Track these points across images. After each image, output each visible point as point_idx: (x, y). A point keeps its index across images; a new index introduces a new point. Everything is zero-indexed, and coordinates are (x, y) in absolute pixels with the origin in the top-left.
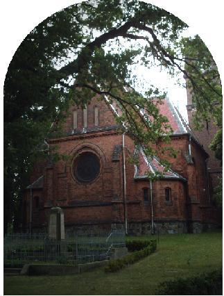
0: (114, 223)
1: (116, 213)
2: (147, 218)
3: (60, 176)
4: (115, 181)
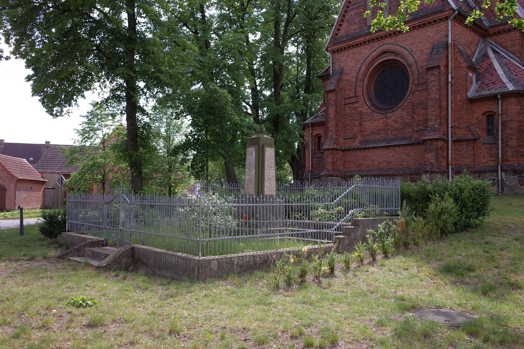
0: (426, 172)
1: (431, 157)
2: (492, 164)
3: (347, 101)
4: (431, 103)
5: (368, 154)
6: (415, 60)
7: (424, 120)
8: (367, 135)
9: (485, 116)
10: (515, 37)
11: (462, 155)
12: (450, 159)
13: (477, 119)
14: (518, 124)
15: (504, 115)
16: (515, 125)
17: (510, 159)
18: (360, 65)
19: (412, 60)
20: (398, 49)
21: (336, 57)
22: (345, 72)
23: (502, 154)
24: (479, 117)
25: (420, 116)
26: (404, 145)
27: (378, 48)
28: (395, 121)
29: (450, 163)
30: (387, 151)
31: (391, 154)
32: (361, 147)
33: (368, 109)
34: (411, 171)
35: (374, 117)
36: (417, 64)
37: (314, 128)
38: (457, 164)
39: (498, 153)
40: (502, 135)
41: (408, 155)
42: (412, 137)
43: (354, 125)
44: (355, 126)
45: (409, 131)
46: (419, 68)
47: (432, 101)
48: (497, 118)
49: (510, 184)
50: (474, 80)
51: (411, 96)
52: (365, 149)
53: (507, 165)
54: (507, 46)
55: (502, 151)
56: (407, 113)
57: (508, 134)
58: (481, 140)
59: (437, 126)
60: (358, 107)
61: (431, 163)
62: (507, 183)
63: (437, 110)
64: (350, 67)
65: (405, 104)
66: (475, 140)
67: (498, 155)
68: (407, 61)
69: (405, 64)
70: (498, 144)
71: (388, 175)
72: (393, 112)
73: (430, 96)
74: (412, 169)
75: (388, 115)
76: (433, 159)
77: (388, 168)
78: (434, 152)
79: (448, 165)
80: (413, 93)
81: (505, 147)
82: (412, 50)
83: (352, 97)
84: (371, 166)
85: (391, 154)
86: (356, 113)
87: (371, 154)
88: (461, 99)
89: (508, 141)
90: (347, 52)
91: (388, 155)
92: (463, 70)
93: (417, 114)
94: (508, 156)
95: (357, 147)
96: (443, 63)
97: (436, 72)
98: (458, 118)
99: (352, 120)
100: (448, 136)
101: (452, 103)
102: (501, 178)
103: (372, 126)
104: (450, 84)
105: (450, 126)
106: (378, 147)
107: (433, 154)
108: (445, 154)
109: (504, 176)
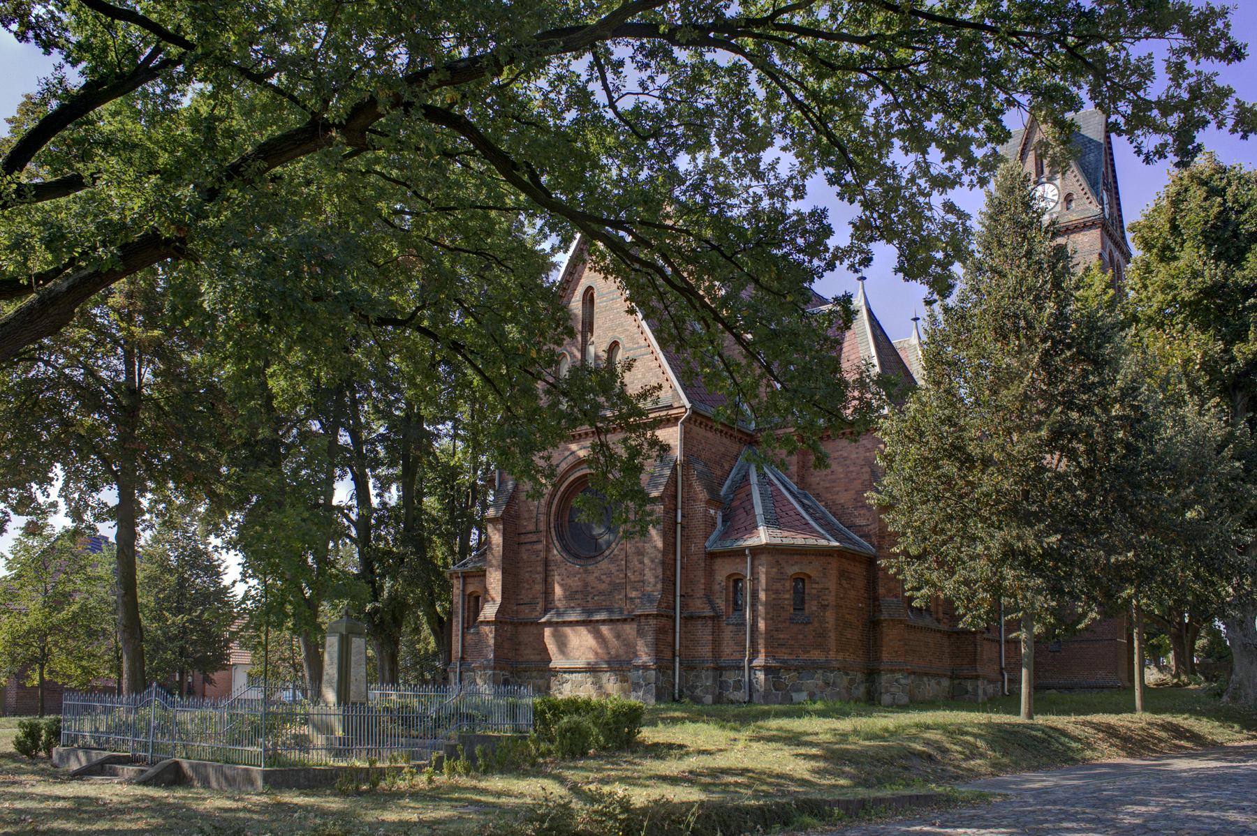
12: (677, 647)
28: (599, 579)
37: (469, 580)
50: (719, 521)
79: (674, 655)
100: (674, 609)
101: (682, 557)
105: (678, 594)
108: (670, 639)
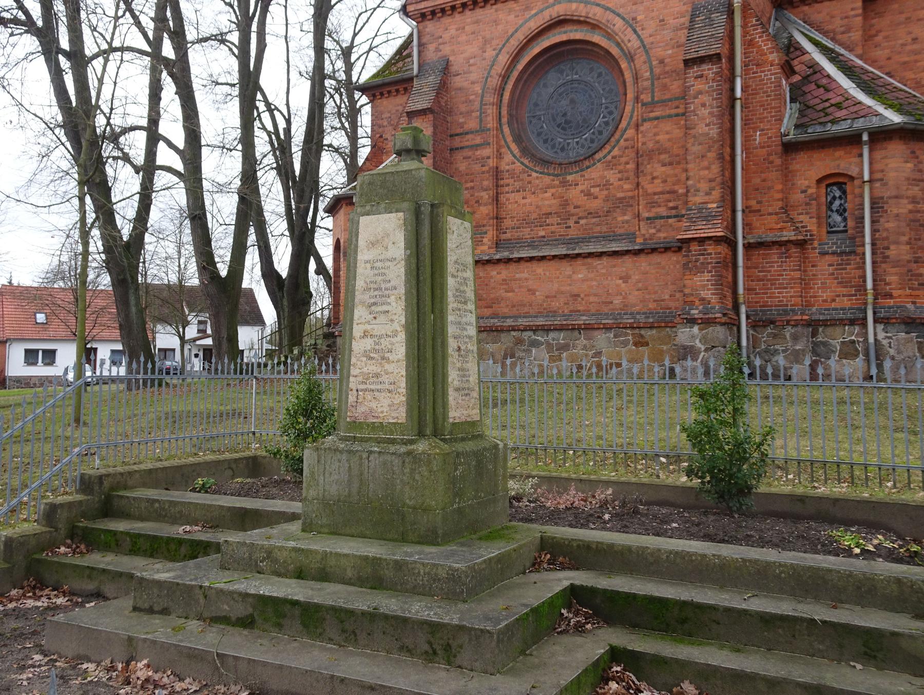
2: (846, 303)
5: (517, 276)
6: (642, 41)
7: (668, 192)
8: (513, 228)
9: (824, 185)
10: (852, 9)
11: (768, 280)
13: (804, 192)
14: (910, 207)
15: (878, 185)
16: (904, 207)
17: (895, 293)
18: (494, 53)
19: (634, 43)
20: (596, 13)
21: (428, 30)
22: (453, 69)
23: (874, 280)
24: (809, 187)
25: (656, 181)
26: (615, 254)
27: (542, 11)
28: (588, 194)
29: (741, 300)
30: (566, 268)
31: (580, 276)
32: (498, 257)
33: (514, 163)
34: (634, 318)
35: (530, 182)
36: (647, 52)
38: (756, 302)
39: (864, 277)
40: (874, 231)
41: (625, 278)
42: (634, 234)
43: (477, 202)
44: (480, 205)
45: (626, 218)
46: (654, 63)
47: (700, 144)
48: (857, 191)
49: (898, 353)
51: (630, 133)
52: (508, 261)
53: (890, 308)
54: (834, 31)
55: (874, 271)
56: (619, 176)
57: (887, 230)
58: (816, 244)
59: (715, 205)
60: (488, 158)
61: (703, 299)
62: (892, 352)
63: (713, 167)
64: (466, 55)
65: (616, 152)
66: (801, 244)
67: (865, 281)
68: (618, 45)
69: (615, 51)
70: (864, 254)
71: (573, 329)
72: (582, 170)
73: (693, 132)
74: (638, 313)
75: (569, 178)
76: (708, 290)
77: (571, 311)
78: (711, 272)
80: (637, 126)
81: (882, 262)
82: (634, 19)
83: (472, 133)
84: (524, 305)
85: (580, 276)
86: (483, 173)
87: (525, 275)
88: (765, 142)
89: (888, 248)
90: (457, 17)
91: (570, 277)
92: (769, 70)
93: (649, 177)
94: (889, 284)
95: (487, 258)
96: (725, 51)
97: (709, 69)
98: (757, 189)
99: (472, 188)
102: (876, 340)
103: (524, 205)
104: (738, 104)
105: (739, 207)
106: (543, 258)
107: (707, 276)
109: (881, 335)
